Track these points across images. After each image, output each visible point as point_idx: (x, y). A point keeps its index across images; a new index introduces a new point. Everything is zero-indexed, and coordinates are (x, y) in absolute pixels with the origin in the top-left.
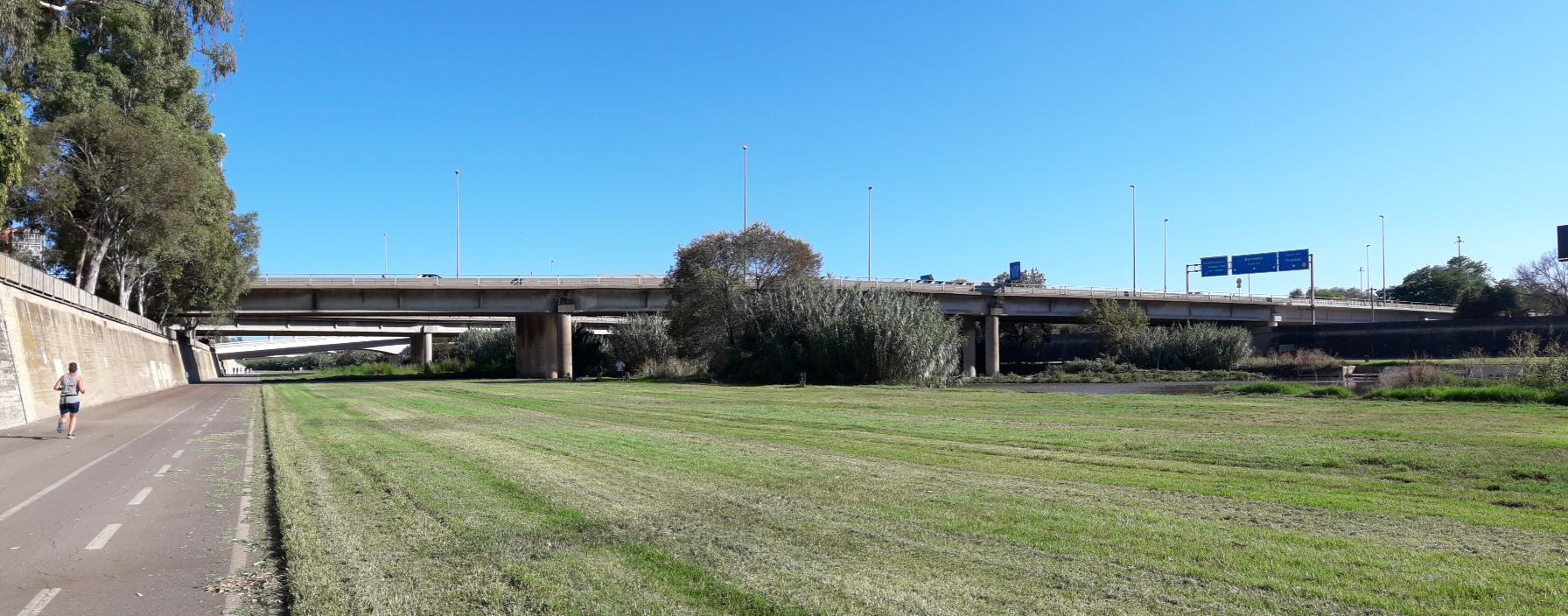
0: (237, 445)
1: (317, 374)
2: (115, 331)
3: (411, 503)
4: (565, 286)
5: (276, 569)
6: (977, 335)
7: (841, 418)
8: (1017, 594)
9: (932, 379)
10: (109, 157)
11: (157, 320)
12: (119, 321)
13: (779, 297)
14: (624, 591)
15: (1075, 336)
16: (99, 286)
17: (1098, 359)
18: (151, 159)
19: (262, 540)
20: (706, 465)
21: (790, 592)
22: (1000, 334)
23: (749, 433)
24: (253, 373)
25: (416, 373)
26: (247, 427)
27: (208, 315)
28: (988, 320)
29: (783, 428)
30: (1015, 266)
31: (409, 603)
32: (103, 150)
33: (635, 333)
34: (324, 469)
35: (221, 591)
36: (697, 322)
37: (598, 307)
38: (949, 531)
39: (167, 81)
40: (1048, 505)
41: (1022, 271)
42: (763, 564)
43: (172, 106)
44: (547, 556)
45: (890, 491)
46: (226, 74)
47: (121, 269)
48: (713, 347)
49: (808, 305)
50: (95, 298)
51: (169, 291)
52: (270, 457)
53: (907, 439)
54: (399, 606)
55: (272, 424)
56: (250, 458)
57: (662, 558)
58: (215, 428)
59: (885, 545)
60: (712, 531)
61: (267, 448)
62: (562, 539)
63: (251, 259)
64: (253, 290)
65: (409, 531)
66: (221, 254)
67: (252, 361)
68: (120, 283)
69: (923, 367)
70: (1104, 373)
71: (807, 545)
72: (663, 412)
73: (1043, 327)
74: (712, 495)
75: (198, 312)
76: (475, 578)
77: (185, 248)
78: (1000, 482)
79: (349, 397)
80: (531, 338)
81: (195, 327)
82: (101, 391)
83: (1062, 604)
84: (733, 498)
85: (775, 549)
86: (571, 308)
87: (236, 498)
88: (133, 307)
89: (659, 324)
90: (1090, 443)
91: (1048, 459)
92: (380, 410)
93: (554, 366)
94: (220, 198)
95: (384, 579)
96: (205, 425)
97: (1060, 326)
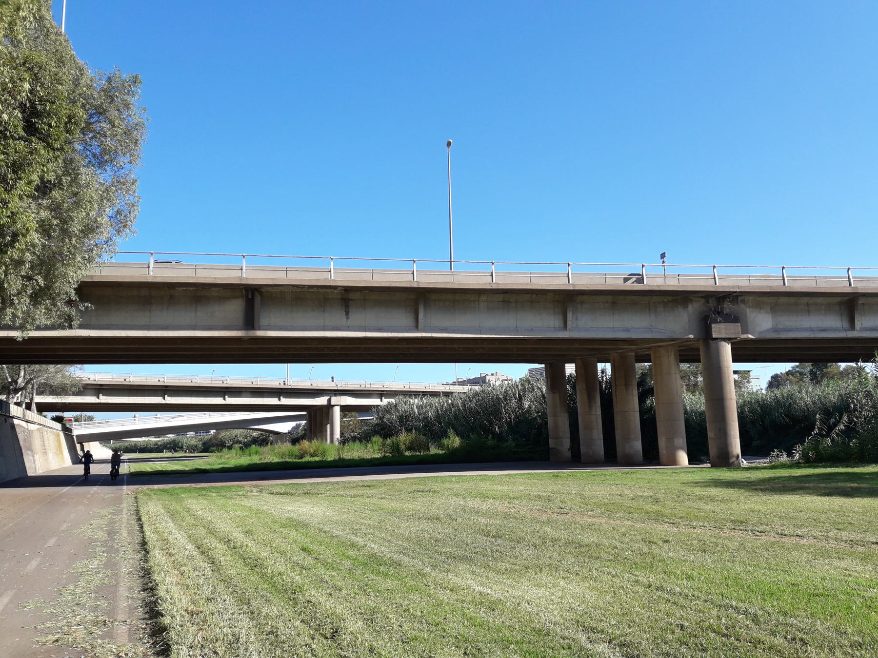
37: (775, 330)
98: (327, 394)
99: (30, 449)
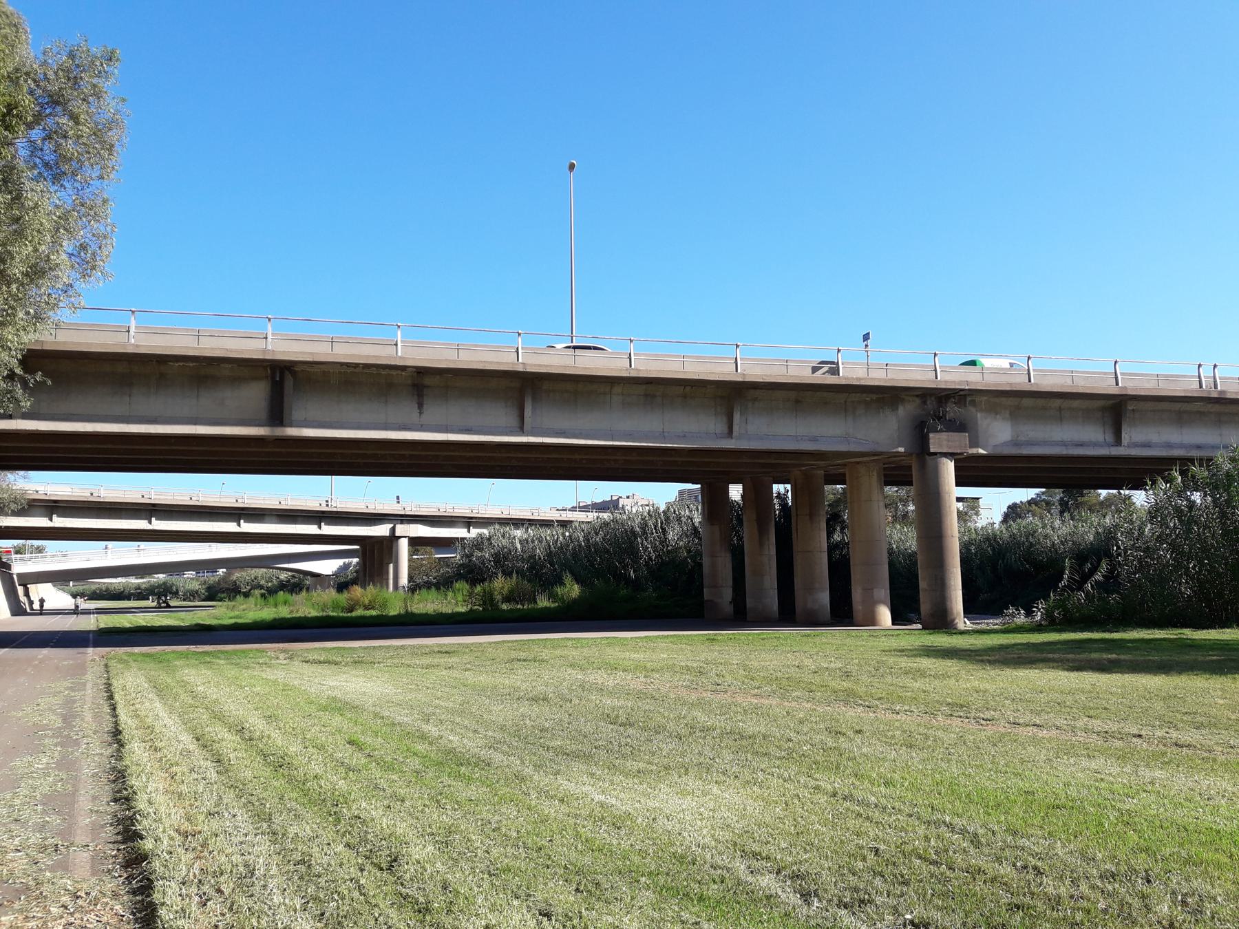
37: (1015, 443)
98: (389, 521)
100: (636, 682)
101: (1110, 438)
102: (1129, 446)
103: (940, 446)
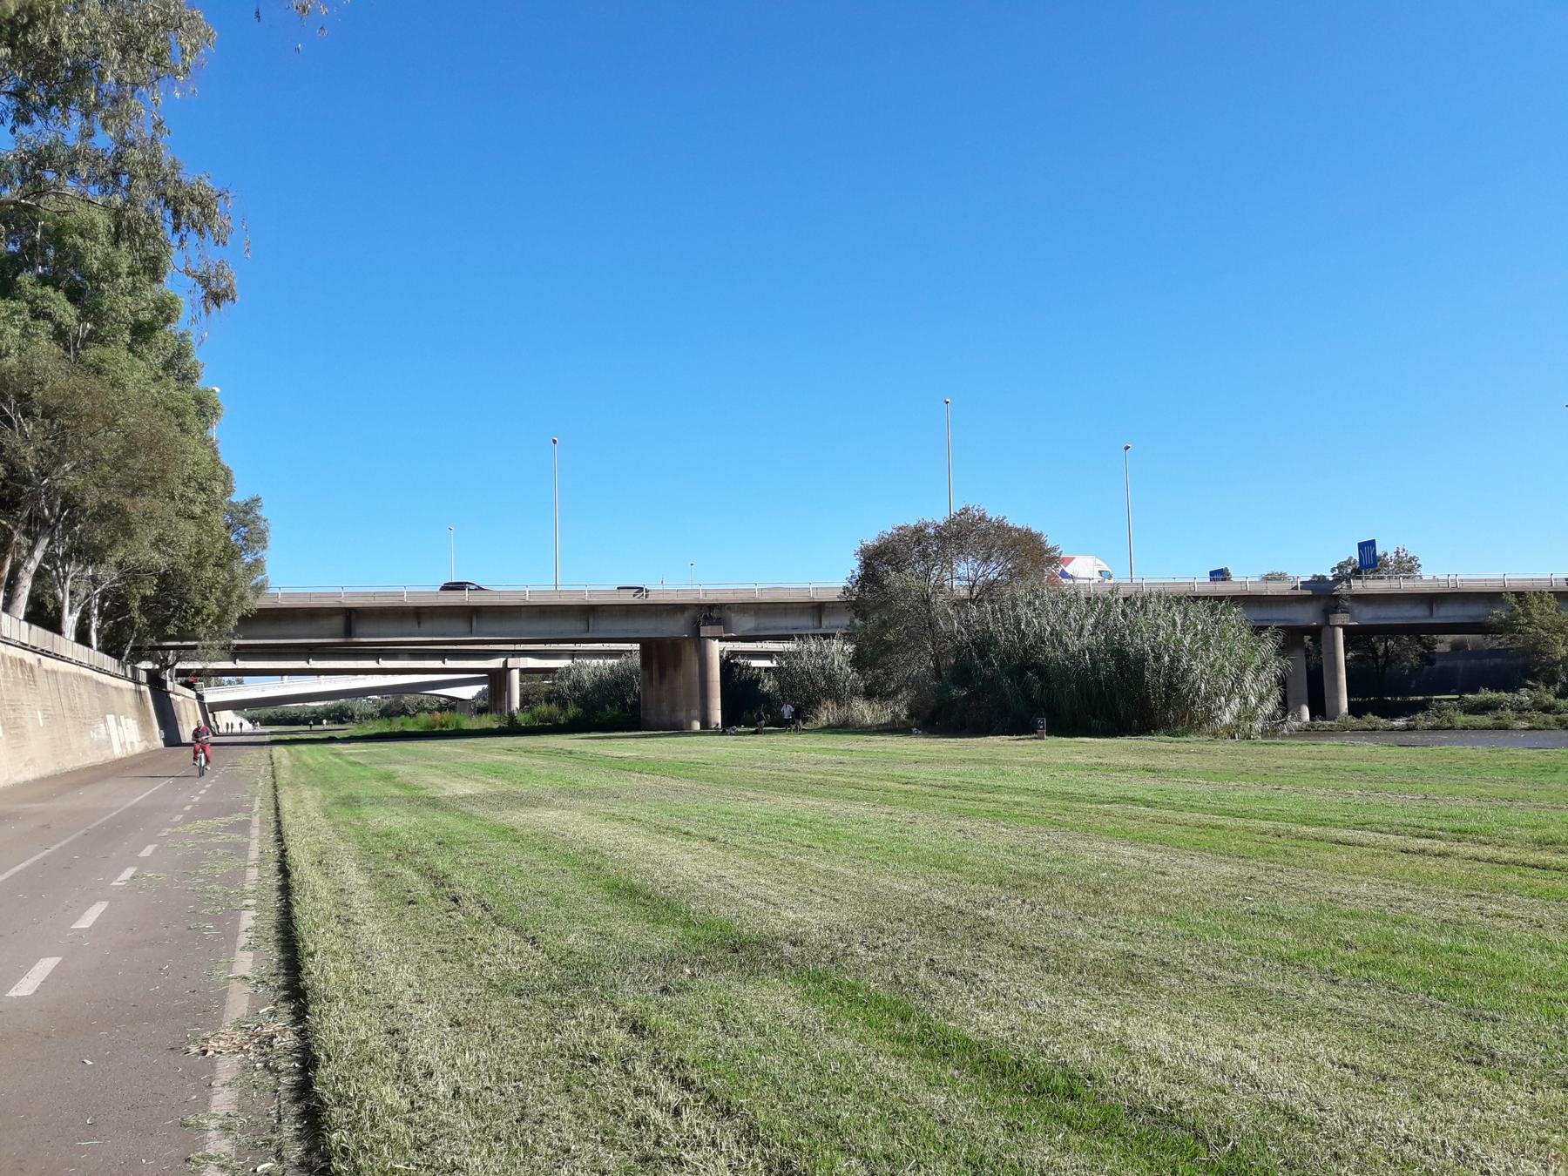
0: (236, 837)
1: (352, 729)
2: (54, 672)
3: (488, 916)
4: (711, 599)
5: (293, 1017)
6: (1307, 657)
7: (1102, 785)
8: (1405, 1067)
9: (1238, 726)
10: (47, 421)
11: (118, 655)
12: (57, 657)
13: (1001, 610)
14: (801, 1036)
15: (1477, 653)
16: (31, 606)
17: (1524, 691)
18: (111, 423)
19: (271, 975)
20: (911, 853)
21: (1043, 1041)
22: (1346, 654)
23: (969, 805)
24: (260, 729)
25: (496, 726)
26: (251, 809)
27: (194, 647)
28: (1325, 633)
29: (1016, 799)
30: (1367, 547)
31: (485, 1062)
32: (38, 411)
33: (806, 663)
34: (362, 869)
35: (210, 1053)
36: (889, 648)
37: (756, 629)
38: (1285, 961)
39: (134, 314)
40: (1450, 929)
41: (1379, 553)
42: (1002, 999)
43: (143, 348)
44: (683, 989)
45: (1188, 898)
46: (222, 304)
47: (65, 582)
48: (914, 683)
49: (1044, 621)
50: (25, 625)
51: (136, 614)
52: (283, 853)
53: (1206, 819)
54: (471, 1067)
55: (287, 804)
56: (254, 854)
57: (853, 988)
58: (204, 811)
59: (1186, 976)
60: (926, 948)
61: (278, 840)
62: (704, 963)
63: (256, 566)
64: (259, 610)
65: (485, 958)
66: (212, 561)
67: (255, 712)
68: (63, 603)
69: (1220, 708)
70: (1535, 714)
71: (1065, 974)
72: (847, 777)
73: (1419, 640)
74: (923, 896)
75: (179, 643)
76: (580, 1024)
77: (160, 551)
78: (1363, 888)
79: (397, 762)
80: (662, 674)
81: (174, 664)
82: (32, 760)
83: (1484, 1090)
84: (951, 901)
85: (1016, 977)
86: (718, 630)
87: (234, 914)
88: (82, 637)
89: (839, 651)
90: (1517, 831)
91: (1443, 855)
92: (443, 781)
93: (696, 712)
94: (213, 479)
95: (449, 1029)
96: (188, 808)
97: (1450, 638)
98: (502, 656)
99: (180, 720)
100: (926, 831)
101: (816, 624)
102: (827, 628)
103: (707, 633)
